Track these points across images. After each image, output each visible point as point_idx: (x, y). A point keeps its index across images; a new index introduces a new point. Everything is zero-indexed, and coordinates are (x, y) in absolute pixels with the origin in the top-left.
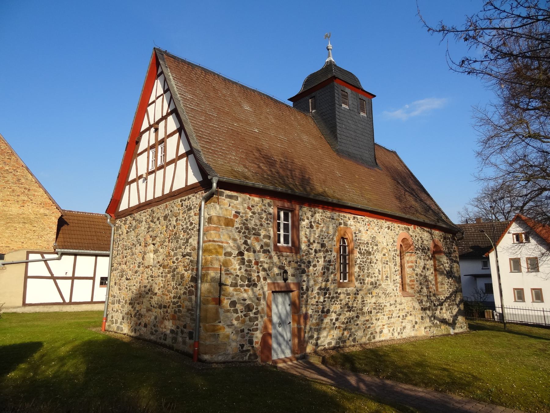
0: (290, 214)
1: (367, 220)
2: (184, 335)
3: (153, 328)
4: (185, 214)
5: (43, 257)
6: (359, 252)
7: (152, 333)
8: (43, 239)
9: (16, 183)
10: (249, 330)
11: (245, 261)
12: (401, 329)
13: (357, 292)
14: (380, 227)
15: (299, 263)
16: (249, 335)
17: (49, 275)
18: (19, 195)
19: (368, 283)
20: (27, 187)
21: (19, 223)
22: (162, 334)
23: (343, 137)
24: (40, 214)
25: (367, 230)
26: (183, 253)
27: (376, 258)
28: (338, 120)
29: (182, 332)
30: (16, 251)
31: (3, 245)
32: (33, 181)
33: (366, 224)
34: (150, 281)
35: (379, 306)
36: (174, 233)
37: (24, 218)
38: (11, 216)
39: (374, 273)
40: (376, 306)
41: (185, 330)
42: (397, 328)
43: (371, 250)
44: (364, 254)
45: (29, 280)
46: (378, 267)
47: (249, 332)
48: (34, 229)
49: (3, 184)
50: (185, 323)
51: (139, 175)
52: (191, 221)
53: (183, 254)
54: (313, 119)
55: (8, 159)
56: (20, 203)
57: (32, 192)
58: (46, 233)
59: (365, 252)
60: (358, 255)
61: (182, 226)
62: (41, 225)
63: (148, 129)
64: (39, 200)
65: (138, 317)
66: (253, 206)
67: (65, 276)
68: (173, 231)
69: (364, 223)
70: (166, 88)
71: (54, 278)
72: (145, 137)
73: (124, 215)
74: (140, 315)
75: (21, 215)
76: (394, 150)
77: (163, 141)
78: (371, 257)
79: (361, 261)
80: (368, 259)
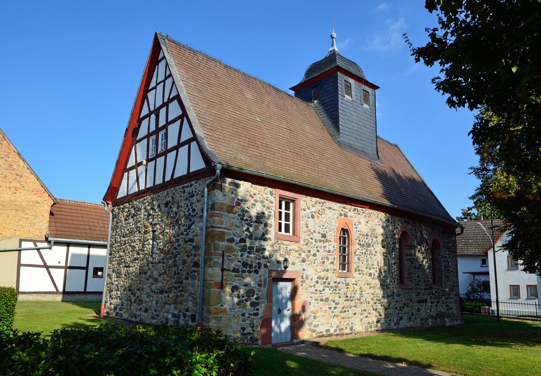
0: (291, 204)
1: (367, 212)
2: (187, 318)
3: (154, 312)
4: (187, 201)
5: (36, 245)
6: (358, 244)
7: (153, 318)
8: (36, 227)
9: (8, 169)
10: (250, 314)
11: (247, 248)
12: (397, 320)
13: (355, 283)
14: (380, 219)
15: (299, 252)
16: (250, 319)
17: (42, 264)
18: (11, 182)
19: (366, 274)
20: (19, 173)
21: (12, 210)
22: (164, 318)
23: (346, 129)
24: (33, 202)
25: (367, 222)
26: (185, 239)
27: (376, 250)
28: (340, 111)
29: (185, 315)
30: (8, 238)
32: (25, 168)
33: (366, 216)
34: (151, 267)
35: (377, 297)
36: (175, 220)
37: (16, 205)
38: (3, 203)
39: (373, 265)
40: (374, 297)
41: (188, 314)
42: (394, 319)
43: (370, 242)
44: (363, 245)
45: (22, 268)
46: (377, 259)
47: (250, 316)
48: (27, 216)
50: (187, 307)
51: (138, 162)
52: (193, 207)
53: (185, 240)
54: (314, 109)
56: (12, 190)
57: (24, 179)
58: (38, 221)
59: (365, 244)
60: (358, 246)
61: (184, 212)
62: (33, 213)
63: (148, 116)
64: (31, 186)
65: (138, 303)
66: (255, 194)
67: (58, 265)
68: (175, 218)
69: (365, 215)
70: (168, 74)
71: (47, 267)
72: (145, 123)
73: (121, 203)
74: (140, 300)
75: (13, 201)
76: (397, 144)
77: (165, 127)
78: (370, 249)
79: (360, 252)
80: (367, 250)
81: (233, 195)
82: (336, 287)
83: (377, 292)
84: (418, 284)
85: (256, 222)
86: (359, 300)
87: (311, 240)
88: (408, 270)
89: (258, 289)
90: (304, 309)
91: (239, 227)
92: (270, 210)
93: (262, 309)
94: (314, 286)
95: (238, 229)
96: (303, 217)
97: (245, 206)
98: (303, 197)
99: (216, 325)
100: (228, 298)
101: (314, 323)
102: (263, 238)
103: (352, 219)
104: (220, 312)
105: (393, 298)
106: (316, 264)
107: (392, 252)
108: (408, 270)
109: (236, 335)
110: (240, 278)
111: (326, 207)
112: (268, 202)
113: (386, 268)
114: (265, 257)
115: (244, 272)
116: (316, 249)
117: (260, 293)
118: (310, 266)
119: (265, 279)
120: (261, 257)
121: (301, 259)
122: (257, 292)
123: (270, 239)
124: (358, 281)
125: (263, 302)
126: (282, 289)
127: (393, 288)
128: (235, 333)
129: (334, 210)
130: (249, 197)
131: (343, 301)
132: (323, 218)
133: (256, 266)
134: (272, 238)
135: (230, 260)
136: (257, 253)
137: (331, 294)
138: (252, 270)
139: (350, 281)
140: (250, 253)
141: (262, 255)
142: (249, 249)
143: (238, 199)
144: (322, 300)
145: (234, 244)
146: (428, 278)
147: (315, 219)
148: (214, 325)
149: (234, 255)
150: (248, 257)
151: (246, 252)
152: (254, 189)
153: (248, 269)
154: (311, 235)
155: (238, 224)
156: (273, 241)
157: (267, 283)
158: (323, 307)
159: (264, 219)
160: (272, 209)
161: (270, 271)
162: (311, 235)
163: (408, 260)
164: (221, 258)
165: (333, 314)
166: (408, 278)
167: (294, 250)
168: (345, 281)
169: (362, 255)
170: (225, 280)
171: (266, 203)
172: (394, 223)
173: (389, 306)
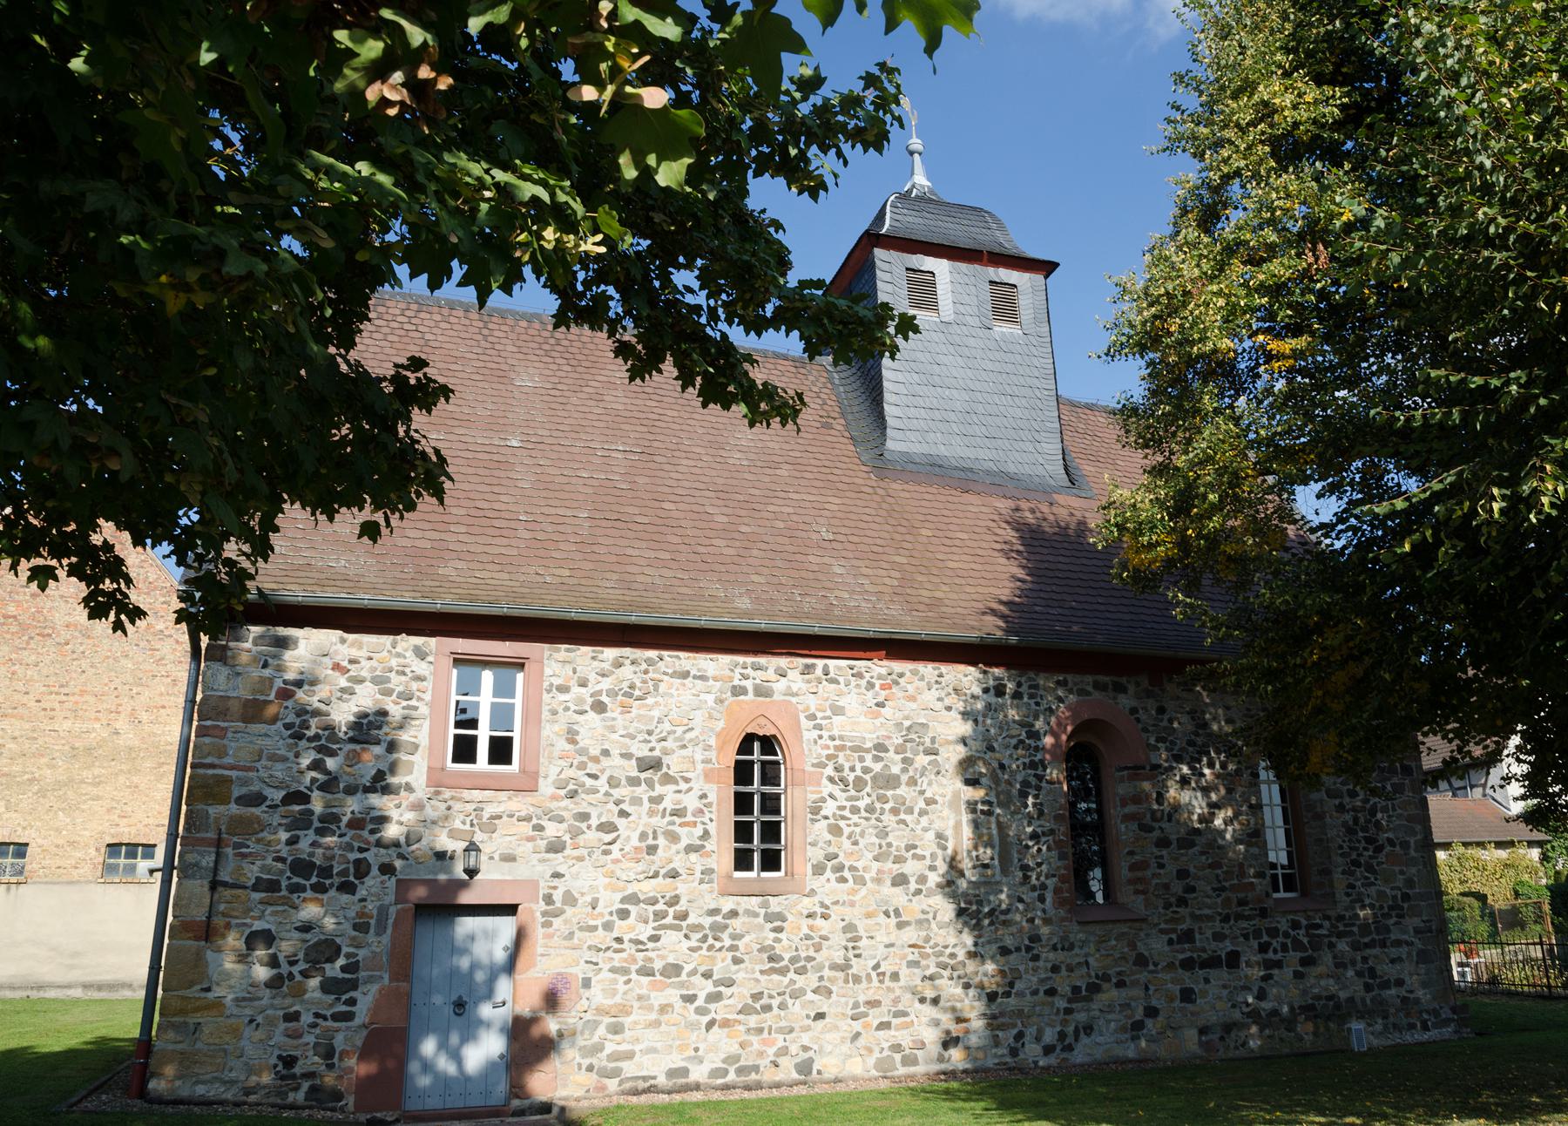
10: (317, 1015)
11: (315, 818)
15: (535, 821)
16: (317, 1031)
31: (151, 821)
47: (320, 1021)
49: (149, 668)
55: (164, 603)
59: (867, 777)
78: (898, 792)
81: (267, 672)
82: (718, 929)
83: (940, 941)
84: (1182, 902)
85: (352, 740)
86: (844, 967)
87: (589, 782)
88: (1131, 853)
89: (353, 938)
90: (551, 1000)
91: (285, 759)
92: (413, 703)
93: (365, 1001)
94: (608, 926)
95: (279, 766)
96: (554, 713)
97: (310, 698)
98: (558, 650)
99: (179, 1047)
100: (229, 964)
101: (610, 1048)
102: (379, 783)
103: (794, 700)
104: (197, 1010)
105: (1036, 958)
106: (616, 854)
107: (1023, 795)
108: (1131, 853)
109: (254, 1078)
110: (280, 908)
111: (665, 673)
112: (403, 678)
113: (986, 853)
114: (385, 841)
115: (295, 889)
116: (616, 810)
117: (362, 954)
118: (587, 862)
119: (383, 911)
120: (368, 843)
121: (543, 844)
122: (351, 950)
123: (409, 788)
124: (836, 903)
125: (370, 980)
126: (472, 938)
127: (1031, 920)
128: (251, 1071)
129: (703, 678)
130: (330, 672)
131: (758, 975)
132: (654, 708)
133: (347, 870)
134: (414, 785)
135: (244, 856)
136: (353, 832)
137: (692, 949)
138: (328, 882)
139: (794, 906)
140: (321, 832)
141: (373, 838)
142: (321, 821)
143: (285, 682)
144: (646, 972)
145: (263, 808)
146: (1242, 874)
147: (608, 714)
148: (171, 1047)
149: (258, 841)
150: (314, 844)
151: (311, 832)
152: (352, 645)
153: (314, 880)
154: (590, 765)
155: (282, 752)
156: (421, 790)
157: (391, 921)
158: (653, 994)
159: (386, 729)
160: (419, 699)
161: (403, 885)
162: (590, 765)
163: (1128, 818)
164: (210, 852)
165: (705, 1019)
166: (1131, 882)
167: (511, 816)
168: (765, 905)
169: (855, 818)
170: (224, 914)
171: (397, 683)
172: (1031, 696)
173: (1011, 985)
